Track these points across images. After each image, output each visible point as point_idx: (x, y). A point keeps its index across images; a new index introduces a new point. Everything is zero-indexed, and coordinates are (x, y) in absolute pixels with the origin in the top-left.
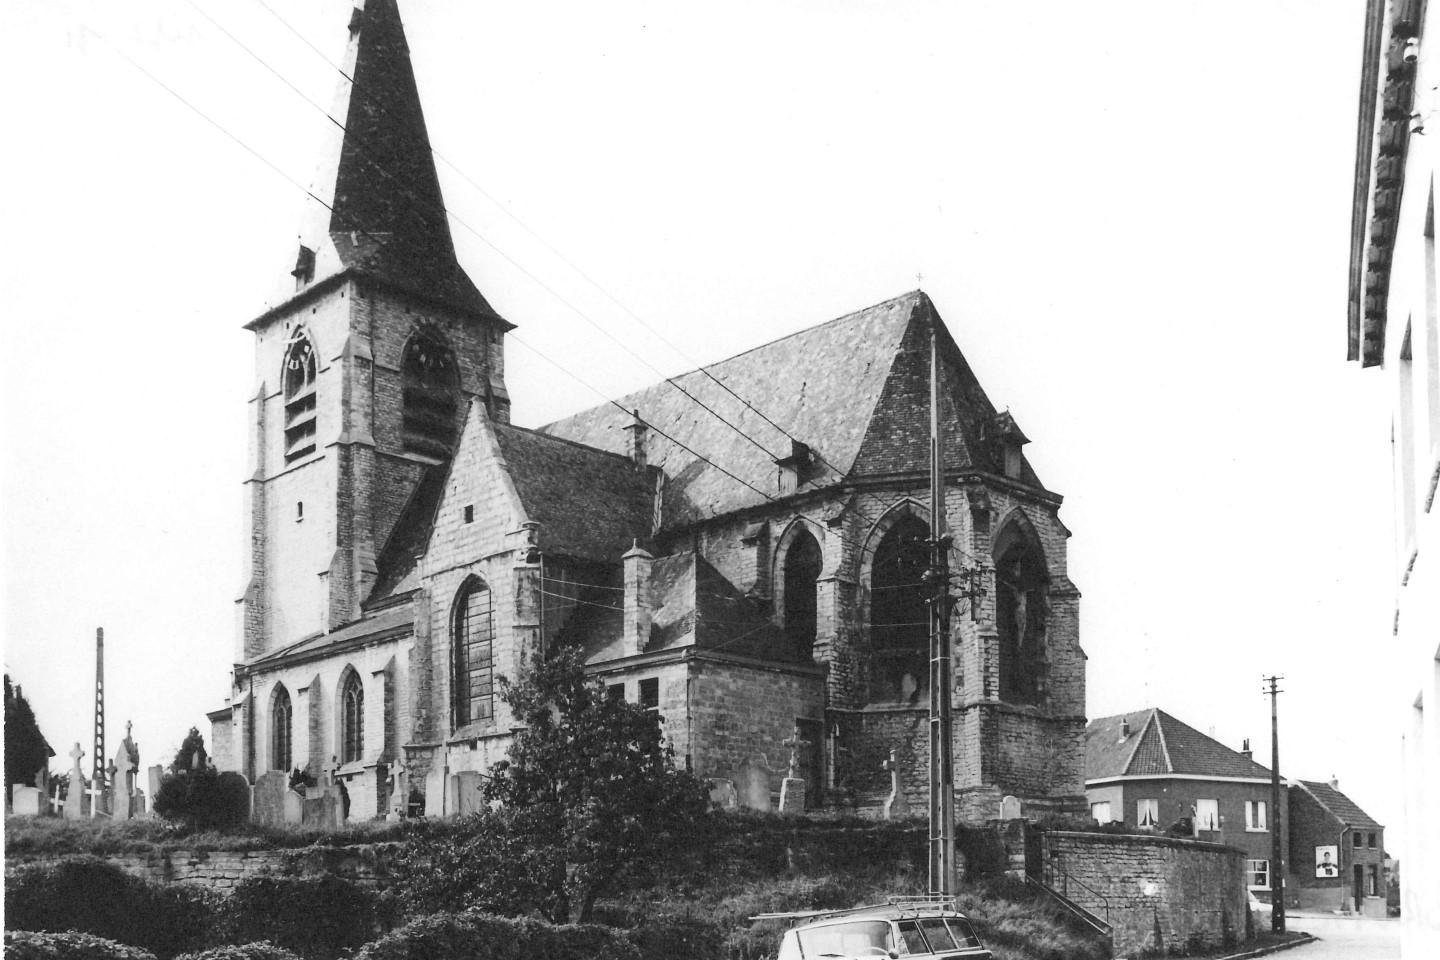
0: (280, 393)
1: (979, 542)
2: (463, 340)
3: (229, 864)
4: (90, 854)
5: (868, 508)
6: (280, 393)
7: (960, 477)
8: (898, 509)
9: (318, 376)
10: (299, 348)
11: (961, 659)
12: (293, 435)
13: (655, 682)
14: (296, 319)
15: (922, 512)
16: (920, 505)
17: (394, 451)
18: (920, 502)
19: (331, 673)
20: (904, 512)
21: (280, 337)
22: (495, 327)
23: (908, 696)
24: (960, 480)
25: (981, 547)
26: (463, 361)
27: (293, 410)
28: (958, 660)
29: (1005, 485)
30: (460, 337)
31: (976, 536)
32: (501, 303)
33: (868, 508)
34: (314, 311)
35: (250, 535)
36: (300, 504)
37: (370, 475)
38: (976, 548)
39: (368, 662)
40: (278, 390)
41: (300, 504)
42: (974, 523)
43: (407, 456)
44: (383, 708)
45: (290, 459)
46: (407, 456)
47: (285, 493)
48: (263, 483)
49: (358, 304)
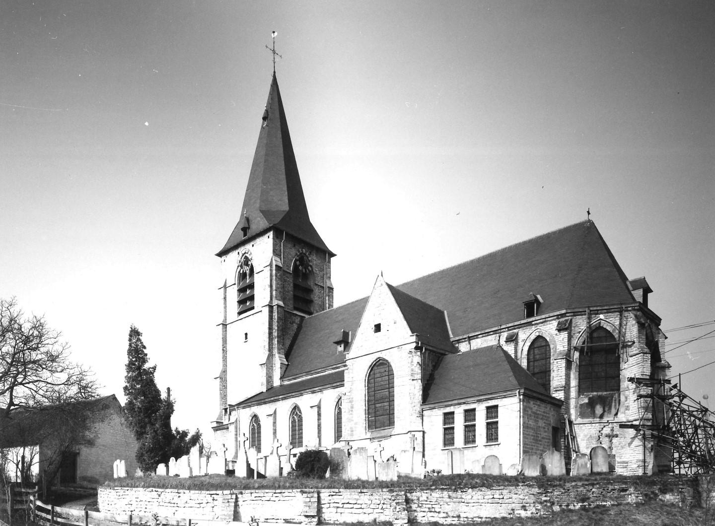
0: (235, 284)
1: (641, 339)
2: (315, 260)
3: (351, 496)
4: (580, 504)
5: (578, 323)
6: (235, 284)
7: (630, 307)
8: (594, 324)
9: (255, 275)
10: (246, 261)
11: (628, 397)
12: (241, 302)
13: (496, 407)
14: (242, 250)
15: (607, 325)
16: (607, 321)
17: (290, 309)
18: (607, 320)
19: (284, 407)
20: (598, 326)
21: (234, 258)
22: (326, 254)
23: (599, 416)
24: (630, 309)
25: (642, 342)
26: (316, 270)
27: (241, 290)
28: (626, 398)
29: (646, 311)
30: (314, 260)
31: (639, 336)
32: (331, 247)
33: (578, 323)
34: (253, 245)
35: (221, 349)
36: (246, 334)
37: (282, 320)
38: (639, 342)
39: (306, 401)
40: (234, 283)
41: (246, 334)
42: (639, 330)
43: (295, 312)
44: (317, 423)
45: (240, 313)
46: (295, 312)
47: (235, 332)
48: (226, 325)
49: (276, 241)
